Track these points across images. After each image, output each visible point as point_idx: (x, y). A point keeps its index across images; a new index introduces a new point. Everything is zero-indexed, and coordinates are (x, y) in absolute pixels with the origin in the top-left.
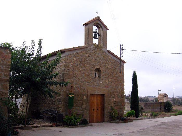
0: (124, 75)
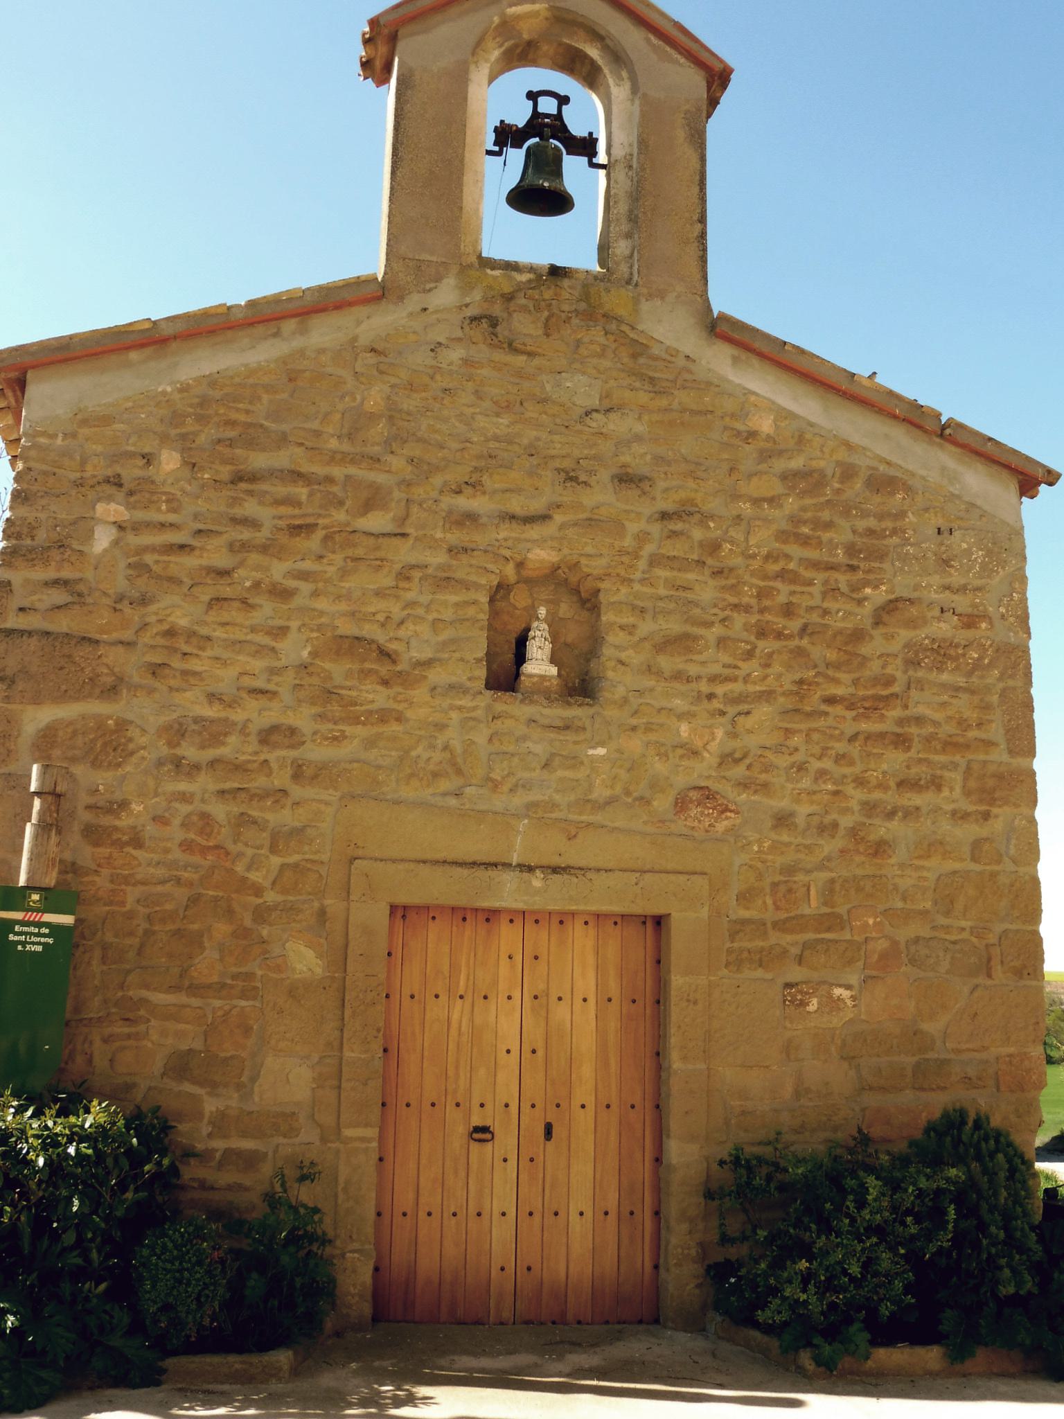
0: (1026, 652)
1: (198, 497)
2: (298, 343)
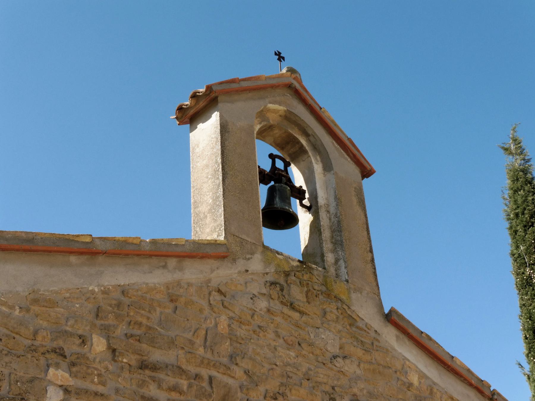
1: (119, 376)
2: (177, 276)
